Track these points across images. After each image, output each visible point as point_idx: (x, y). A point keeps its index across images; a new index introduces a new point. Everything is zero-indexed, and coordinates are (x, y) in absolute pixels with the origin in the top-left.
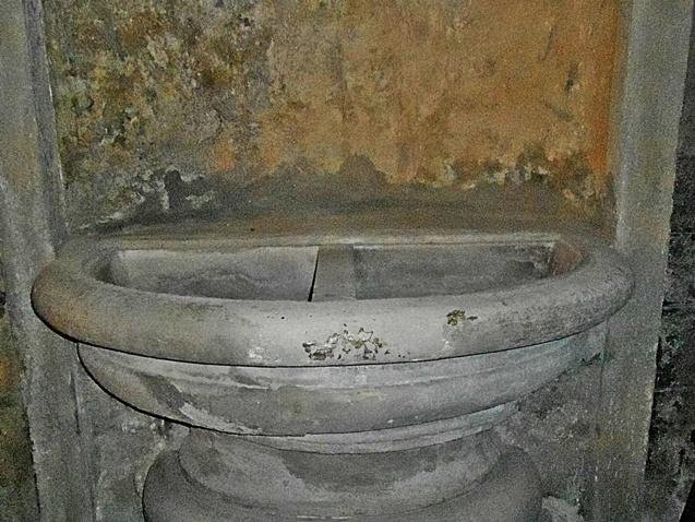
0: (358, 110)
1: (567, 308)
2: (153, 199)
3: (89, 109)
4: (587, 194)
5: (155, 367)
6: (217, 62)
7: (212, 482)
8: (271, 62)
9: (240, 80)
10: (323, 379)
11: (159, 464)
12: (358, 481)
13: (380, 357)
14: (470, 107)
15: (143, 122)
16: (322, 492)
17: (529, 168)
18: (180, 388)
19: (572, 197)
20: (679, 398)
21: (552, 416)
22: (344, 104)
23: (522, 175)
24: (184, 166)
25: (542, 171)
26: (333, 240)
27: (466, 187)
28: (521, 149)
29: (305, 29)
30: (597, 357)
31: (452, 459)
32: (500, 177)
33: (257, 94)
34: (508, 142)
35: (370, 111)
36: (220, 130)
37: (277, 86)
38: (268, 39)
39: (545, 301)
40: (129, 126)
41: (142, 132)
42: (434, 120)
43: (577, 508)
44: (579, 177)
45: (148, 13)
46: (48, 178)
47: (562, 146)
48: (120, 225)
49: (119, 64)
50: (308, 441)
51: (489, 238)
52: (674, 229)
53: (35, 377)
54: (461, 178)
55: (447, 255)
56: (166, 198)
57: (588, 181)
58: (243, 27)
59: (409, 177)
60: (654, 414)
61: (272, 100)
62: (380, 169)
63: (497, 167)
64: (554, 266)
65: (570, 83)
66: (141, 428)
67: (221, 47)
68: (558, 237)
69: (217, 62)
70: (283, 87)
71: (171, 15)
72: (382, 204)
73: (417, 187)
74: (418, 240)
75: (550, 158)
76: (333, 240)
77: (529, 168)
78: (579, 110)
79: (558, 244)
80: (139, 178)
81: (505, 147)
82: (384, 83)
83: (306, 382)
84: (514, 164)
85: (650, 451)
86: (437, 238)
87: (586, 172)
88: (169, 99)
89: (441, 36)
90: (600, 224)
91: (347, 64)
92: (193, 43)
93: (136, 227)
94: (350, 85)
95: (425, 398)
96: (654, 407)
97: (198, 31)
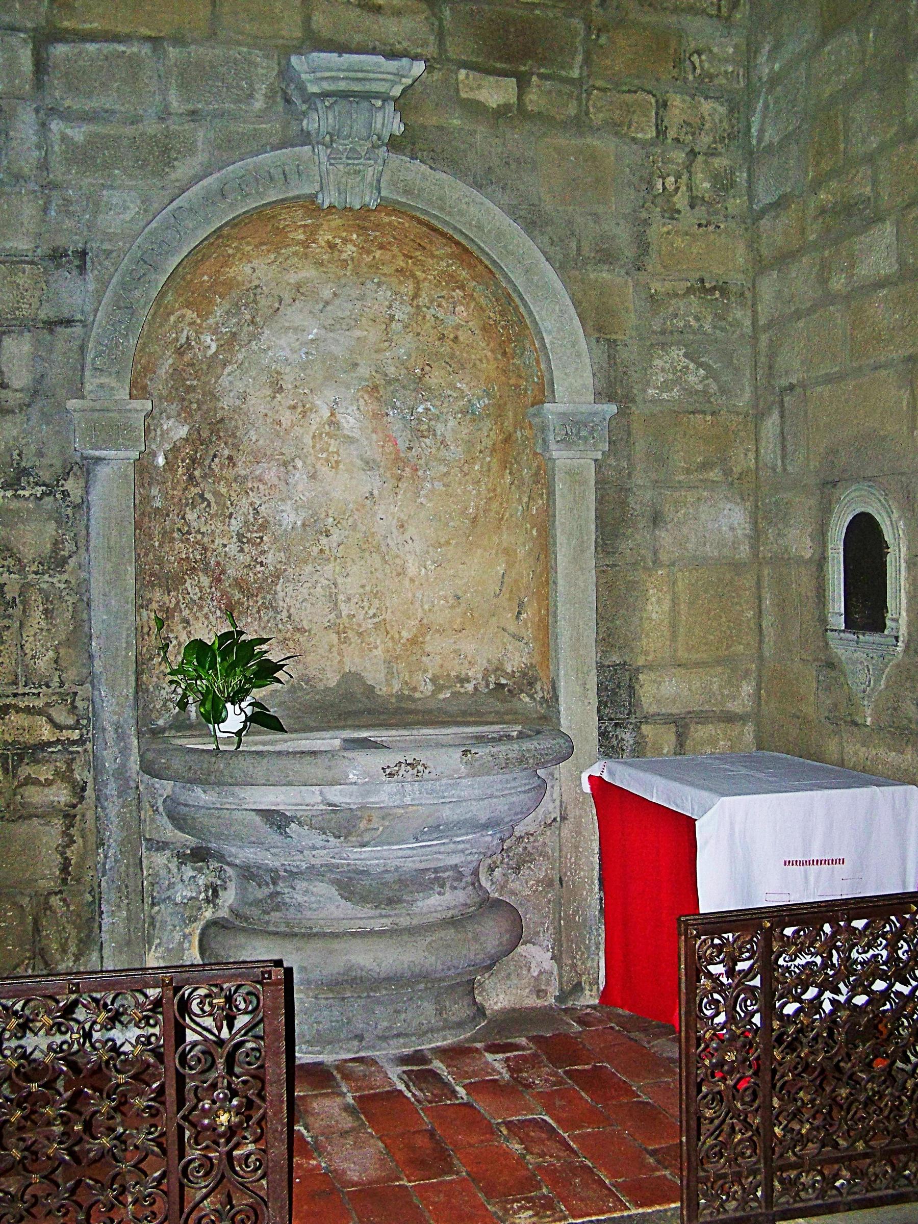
0: (350, 634)
4: (538, 697)
6: (237, 596)
8: (281, 594)
9: (255, 610)
14: (441, 631)
16: (366, 910)
17: (492, 679)
18: (288, 814)
19: (527, 699)
21: (525, 871)
23: (487, 686)
25: (503, 681)
29: (309, 568)
30: (555, 819)
31: (455, 888)
32: (470, 687)
33: (268, 621)
34: (475, 654)
35: (360, 634)
37: (284, 614)
38: (278, 578)
42: (413, 641)
43: (550, 954)
44: (531, 684)
45: (188, 558)
47: (515, 661)
49: (166, 598)
53: (111, 852)
54: (439, 688)
57: (538, 686)
58: (259, 568)
59: (396, 687)
61: (280, 626)
63: (468, 680)
65: (519, 613)
66: (191, 899)
67: (238, 584)
68: (519, 728)
70: (289, 617)
75: (509, 670)
77: (492, 679)
78: (529, 634)
82: (371, 612)
83: (373, 803)
84: (480, 676)
86: (431, 731)
87: (536, 679)
91: (341, 597)
92: (219, 580)
97: (223, 572)
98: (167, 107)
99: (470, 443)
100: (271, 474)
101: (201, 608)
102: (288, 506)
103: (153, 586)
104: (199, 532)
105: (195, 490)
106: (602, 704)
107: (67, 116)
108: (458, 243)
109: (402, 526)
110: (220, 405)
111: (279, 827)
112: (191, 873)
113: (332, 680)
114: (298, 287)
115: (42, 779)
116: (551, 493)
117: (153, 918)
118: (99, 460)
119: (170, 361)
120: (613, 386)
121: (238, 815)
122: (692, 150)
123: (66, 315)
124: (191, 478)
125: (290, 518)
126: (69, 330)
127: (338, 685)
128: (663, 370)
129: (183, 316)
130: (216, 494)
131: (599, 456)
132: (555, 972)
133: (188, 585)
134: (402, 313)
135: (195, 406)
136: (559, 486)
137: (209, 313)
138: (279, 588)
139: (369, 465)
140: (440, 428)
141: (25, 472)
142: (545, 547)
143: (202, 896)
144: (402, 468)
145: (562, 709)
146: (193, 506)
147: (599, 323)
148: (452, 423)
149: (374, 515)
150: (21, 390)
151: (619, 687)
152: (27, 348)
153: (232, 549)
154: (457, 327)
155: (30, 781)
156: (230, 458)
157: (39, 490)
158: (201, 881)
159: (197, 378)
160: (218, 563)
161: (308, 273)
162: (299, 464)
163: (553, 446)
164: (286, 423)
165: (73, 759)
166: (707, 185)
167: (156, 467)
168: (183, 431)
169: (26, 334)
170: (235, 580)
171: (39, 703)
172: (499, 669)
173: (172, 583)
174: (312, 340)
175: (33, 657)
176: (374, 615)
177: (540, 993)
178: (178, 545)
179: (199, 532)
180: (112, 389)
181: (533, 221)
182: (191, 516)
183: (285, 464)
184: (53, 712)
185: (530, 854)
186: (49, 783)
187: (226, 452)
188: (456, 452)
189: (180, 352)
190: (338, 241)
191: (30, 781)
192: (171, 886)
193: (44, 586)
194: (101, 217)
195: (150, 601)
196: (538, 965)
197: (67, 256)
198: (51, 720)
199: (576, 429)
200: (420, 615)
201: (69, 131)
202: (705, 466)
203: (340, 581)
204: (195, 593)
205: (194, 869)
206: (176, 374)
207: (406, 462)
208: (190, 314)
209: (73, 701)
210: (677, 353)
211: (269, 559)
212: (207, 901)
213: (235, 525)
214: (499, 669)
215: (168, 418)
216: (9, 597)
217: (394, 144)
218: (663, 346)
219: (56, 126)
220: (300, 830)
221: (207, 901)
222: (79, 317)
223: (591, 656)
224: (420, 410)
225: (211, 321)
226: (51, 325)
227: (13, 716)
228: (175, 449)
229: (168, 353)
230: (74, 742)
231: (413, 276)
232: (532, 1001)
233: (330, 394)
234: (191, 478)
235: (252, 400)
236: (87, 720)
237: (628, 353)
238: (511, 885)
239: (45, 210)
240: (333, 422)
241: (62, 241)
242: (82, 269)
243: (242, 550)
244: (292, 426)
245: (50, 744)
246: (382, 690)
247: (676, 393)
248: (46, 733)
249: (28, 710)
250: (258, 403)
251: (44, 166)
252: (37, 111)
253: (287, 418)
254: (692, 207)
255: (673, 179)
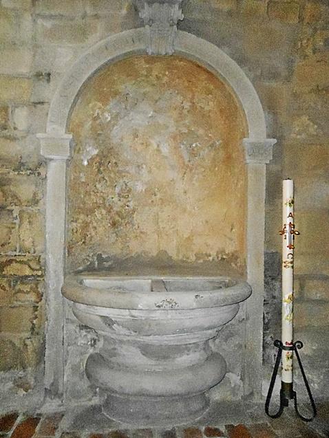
1: (229, 296)
2: (92, 263)
3: (76, 232)
4: (239, 265)
5: (106, 312)
6: (117, 218)
7: (113, 359)
10: (158, 315)
11: (91, 357)
12: (165, 358)
13: (176, 307)
15: (92, 237)
17: (220, 256)
19: (234, 265)
20: (272, 335)
22: (159, 234)
23: (218, 257)
24: (103, 252)
25: (224, 257)
26: (155, 278)
27: (199, 262)
28: (217, 249)
29: (147, 208)
32: (211, 258)
34: (213, 245)
36: (117, 240)
37: (136, 226)
39: (223, 293)
40: (87, 238)
41: (91, 240)
43: (239, 377)
46: (65, 254)
47: (230, 248)
48: (81, 271)
50: (147, 339)
51: (206, 278)
52: (265, 276)
55: (193, 283)
56: (96, 263)
58: (127, 207)
59: (181, 257)
60: (264, 340)
62: (170, 255)
63: (210, 256)
64: (227, 286)
65: (232, 229)
66: (84, 344)
67: (118, 213)
69: (117, 218)
71: (104, 203)
72: (171, 267)
73: (183, 262)
74: (184, 278)
76: (155, 278)
77: (220, 256)
79: (229, 280)
80: (88, 256)
81: (212, 249)
85: (263, 355)
88: (101, 230)
89: (190, 212)
90: (243, 274)
92: (110, 212)
93: (86, 273)
94: (161, 227)
95: (188, 324)
96: (264, 337)
97: (111, 208)
98: (86, 12)
99: (214, 159)
100: (132, 170)
101: (102, 222)
102: (139, 183)
103: (79, 213)
104: (102, 192)
105: (100, 176)
106: (266, 270)
107: (44, 17)
108: (208, 72)
109: (185, 192)
110: (111, 141)
111: (109, 325)
112: (85, 333)
113: (154, 253)
114: (145, 94)
115: (25, 291)
116: (246, 179)
117: (68, 352)
118: (51, 160)
119: (90, 123)
120: (276, 131)
121: (92, 317)
122: (315, 28)
123: (42, 100)
124: (99, 170)
125: (140, 188)
126: (43, 106)
127: (157, 255)
128: (298, 125)
129: (96, 105)
130: (110, 177)
131: (268, 162)
132: (242, 386)
133: (96, 213)
134: (187, 105)
135: (101, 142)
136: (249, 175)
137: (107, 105)
138: (135, 215)
139: (173, 167)
140: (202, 153)
141: (23, 164)
142: (243, 203)
143: (89, 343)
144: (187, 169)
145: (248, 272)
146: (100, 182)
147: (270, 104)
148: (207, 150)
149: (174, 188)
150: (23, 131)
151: (274, 262)
152: (25, 113)
153: (116, 199)
154: (210, 111)
155: (20, 291)
156: (116, 163)
157: (29, 172)
158: (89, 336)
159: (102, 130)
160: (110, 205)
161: (148, 89)
162: (144, 166)
163: (247, 157)
164: (139, 150)
165: (38, 283)
166: (322, 43)
167: (83, 165)
168: (96, 152)
169: (25, 107)
170: (117, 212)
171: (25, 260)
172: (223, 251)
173: (91, 212)
174: (150, 117)
175: (23, 240)
176: (173, 228)
177: (234, 394)
178: (92, 197)
179: (102, 192)
180: (58, 130)
181: (241, 61)
182: (98, 186)
183: (139, 166)
184: (31, 264)
185: (232, 333)
186: (28, 293)
187: (114, 161)
188: (208, 162)
189: (95, 119)
190: (160, 75)
191: (20, 291)
192: (76, 338)
193: (29, 211)
194: (57, 60)
195: (78, 219)
196: (234, 382)
197: (42, 75)
198: (30, 267)
199: (257, 149)
200: (191, 228)
201: (45, 24)
202: (315, 168)
203: (160, 213)
204: (99, 216)
205: (86, 332)
206: (93, 128)
207: (188, 166)
208: (100, 104)
209: (39, 260)
210: (305, 118)
211: (131, 204)
212: (92, 345)
213: (117, 190)
214: (223, 251)
215: (90, 146)
216: (15, 215)
217: (181, 25)
218: (298, 116)
219: (40, 21)
220: (118, 327)
221: (92, 345)
222: (47, 101)
223: (262, 249)
224: (194, 145)
225: (108, 107)
226: (35, 104)
227: (14, 264)
228: (92, 159)
229: (89, 120)
230: (39, 276)
231: (192, 90)
232: (230, 398)
233: (157, 138)
234: (99, 170)
235: (125, 141)
236: (43, 267)
237: (283, 119)
238: (224, 347)
239: (34, 56)
240: (158, 150)
241: (40, 69)
242: (48, 81)
243: (120, 200)
244: (142, 151)
245: (28, 276)
246: (175, 257)
247: (303, 136)
248: (28, 272)
249: (21, 262)
250: (128, 141)
251: (34, 38)
252: (32, 15)
253: (139, 148)
254: (314, 53)
255: (305, 41)
